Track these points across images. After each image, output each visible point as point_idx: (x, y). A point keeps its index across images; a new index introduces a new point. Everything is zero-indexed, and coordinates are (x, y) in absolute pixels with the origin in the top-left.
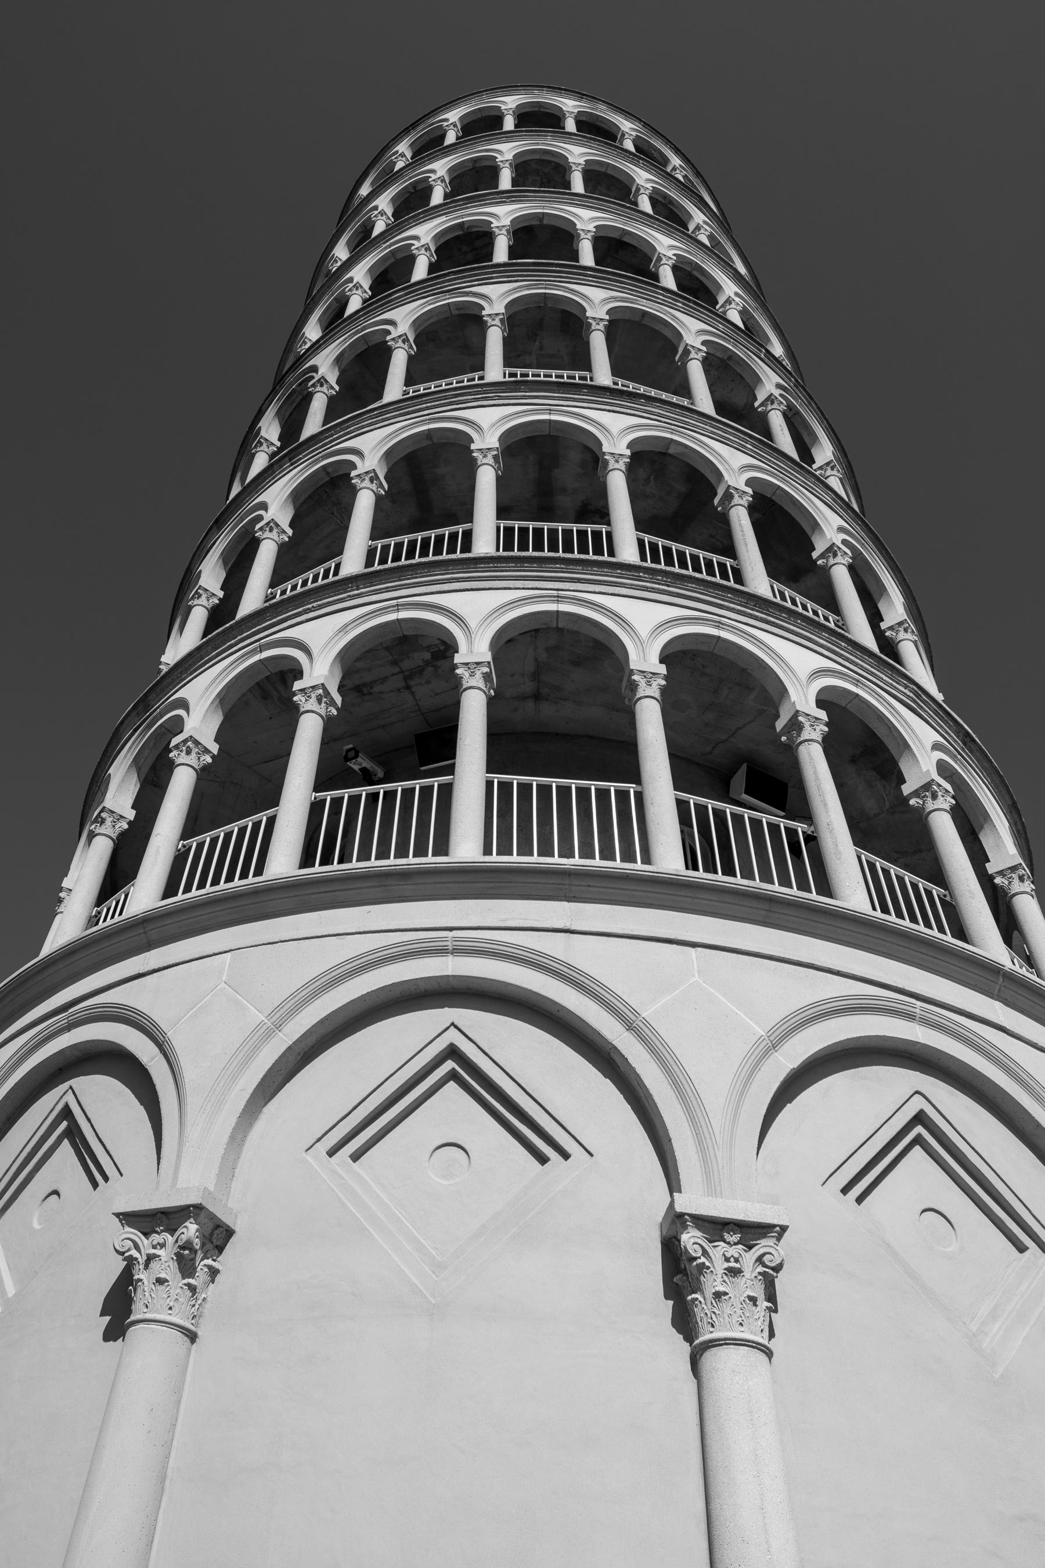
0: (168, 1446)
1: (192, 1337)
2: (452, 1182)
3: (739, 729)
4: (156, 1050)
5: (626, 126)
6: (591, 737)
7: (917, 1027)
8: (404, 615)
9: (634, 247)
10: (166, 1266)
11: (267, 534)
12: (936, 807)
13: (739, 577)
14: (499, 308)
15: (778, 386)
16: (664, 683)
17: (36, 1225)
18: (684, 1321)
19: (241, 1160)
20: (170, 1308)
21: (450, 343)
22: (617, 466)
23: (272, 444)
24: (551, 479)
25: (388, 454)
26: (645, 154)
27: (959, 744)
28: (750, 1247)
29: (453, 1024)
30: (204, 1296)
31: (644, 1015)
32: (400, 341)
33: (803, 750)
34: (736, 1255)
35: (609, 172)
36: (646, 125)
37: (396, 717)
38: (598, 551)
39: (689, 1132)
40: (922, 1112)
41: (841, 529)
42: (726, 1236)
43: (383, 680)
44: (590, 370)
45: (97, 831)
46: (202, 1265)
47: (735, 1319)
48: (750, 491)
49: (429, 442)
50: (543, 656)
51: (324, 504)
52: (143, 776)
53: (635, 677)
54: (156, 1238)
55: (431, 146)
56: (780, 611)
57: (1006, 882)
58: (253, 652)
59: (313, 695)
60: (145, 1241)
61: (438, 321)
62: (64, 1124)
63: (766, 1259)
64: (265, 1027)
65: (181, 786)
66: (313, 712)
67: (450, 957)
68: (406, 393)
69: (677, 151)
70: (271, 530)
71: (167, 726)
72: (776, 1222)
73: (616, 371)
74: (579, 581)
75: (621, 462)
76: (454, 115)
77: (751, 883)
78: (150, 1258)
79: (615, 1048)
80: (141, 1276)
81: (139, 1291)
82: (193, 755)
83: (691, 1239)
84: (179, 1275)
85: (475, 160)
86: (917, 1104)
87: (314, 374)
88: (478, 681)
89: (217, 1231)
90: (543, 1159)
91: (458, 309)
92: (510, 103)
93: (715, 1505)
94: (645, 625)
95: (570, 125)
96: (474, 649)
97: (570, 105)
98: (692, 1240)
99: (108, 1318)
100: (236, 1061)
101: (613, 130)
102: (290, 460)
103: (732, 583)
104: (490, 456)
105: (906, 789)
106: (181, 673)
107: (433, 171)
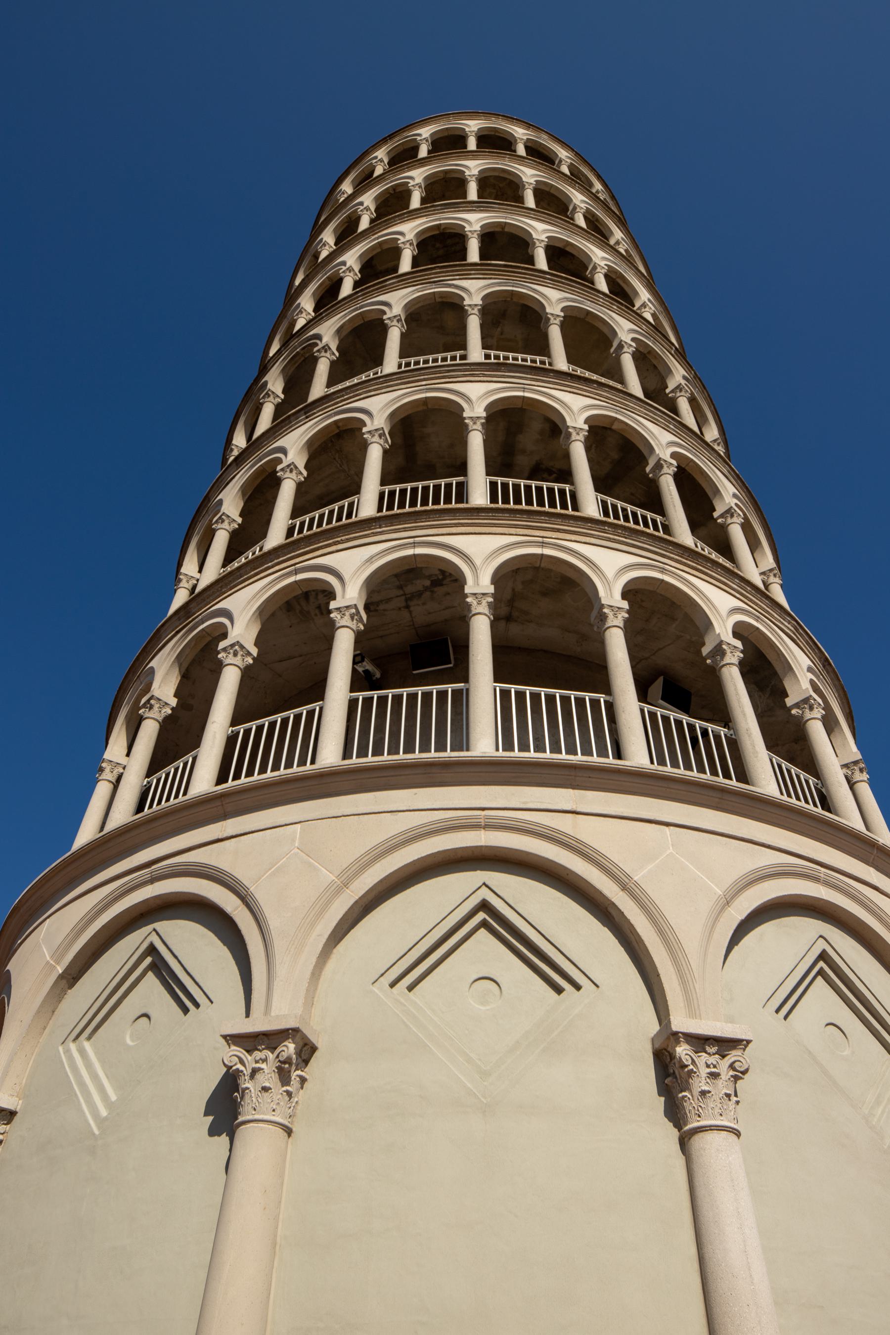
0: (276, 1219)
1: (289, 1132)
2: (488, 1007)
3: (660, 649)
4: (239, 902)
5: (563, 154)
6: (545, 651)
7: (821, 887)
8: (419, 551)
9: (573, 255)
10: (268, 1076)
11: (288, 474)
12: (812, 716)
13: (667, 529)
14: (477, 300)
15: (684, 378)
16: (627, 615)
17: (129, 1042)
18: (675, 1112)
19: (318, 991)
20: (274, 1110)
21: (435, 326)
22: (578, 438)
23: (278, 396)
24: (525, 444)
25: (392, 415)
26: (576, 178)
27: (821, 667)
28: (723, 1057)
29: (484, 884)
30: (296, 1099)
31: (635, 879)
32: (395, 321)
33: (725, 671)
34: (715, 1063)
35: (552, 191)
36: (577, 154)
37: (414, 640)
38: (564, 506)
39: (672, 969)
40: (824, 951)
41: (735, 496)
42: (708, 1049)
43: (389, 600)
44: (549, 356)
45: (146, 715)
46: (295, 1074)
47: (717, 1110)
48: (674, 462)
49: (425, 408)
50: (519, 587)
51: (336, 455)
52: (183, 670)
53: (605, 610)
54: (258, 1055)
55: (406, 156)
56: (706, 561)
57: (850, 773)
58: (289, 574)
59: (347, 614)
60: (249, 1058)
61: (423, 306)
62: (149, 960)
63: (737, 1065)
64: (335, 885)
65: (229, 683)
66: (347, 627)
67: (483, 831)
68: (400, 366)
69: (599, 178)
70: (291, 471)
71: (207, 630)
72: (743, 1037)
73: (570, 360)
74: (558, 530)
75: (581, 435)
76: (426, 132)
77: (676, 770)
78: (254, 1072)
79: (613, 904)
80: (247, 1085)
81: (247, 1097)
82: (239, 657)
83: (683, 1051)
84: (279, 1084)
85: (446, 172)
86: (821, 945)
87: (318, 342)
88: (484, 608)
89: (305, 1048)
90: (559, 990)
91: (441, 297)
92: (473, 126)
93: (708, 1251)
94: (610, 568)
95: (521, 150)
96: (479, 583)
97: (520, 133)
98: (685, 1052)
99: (211, 1118)
100: (313, 912)
101: (552, 156)
102: (305, 413)
103: (661, 534)
104: (479, 423)
105: (789, 702)
106: (221, 587)
107: (412, 178)
